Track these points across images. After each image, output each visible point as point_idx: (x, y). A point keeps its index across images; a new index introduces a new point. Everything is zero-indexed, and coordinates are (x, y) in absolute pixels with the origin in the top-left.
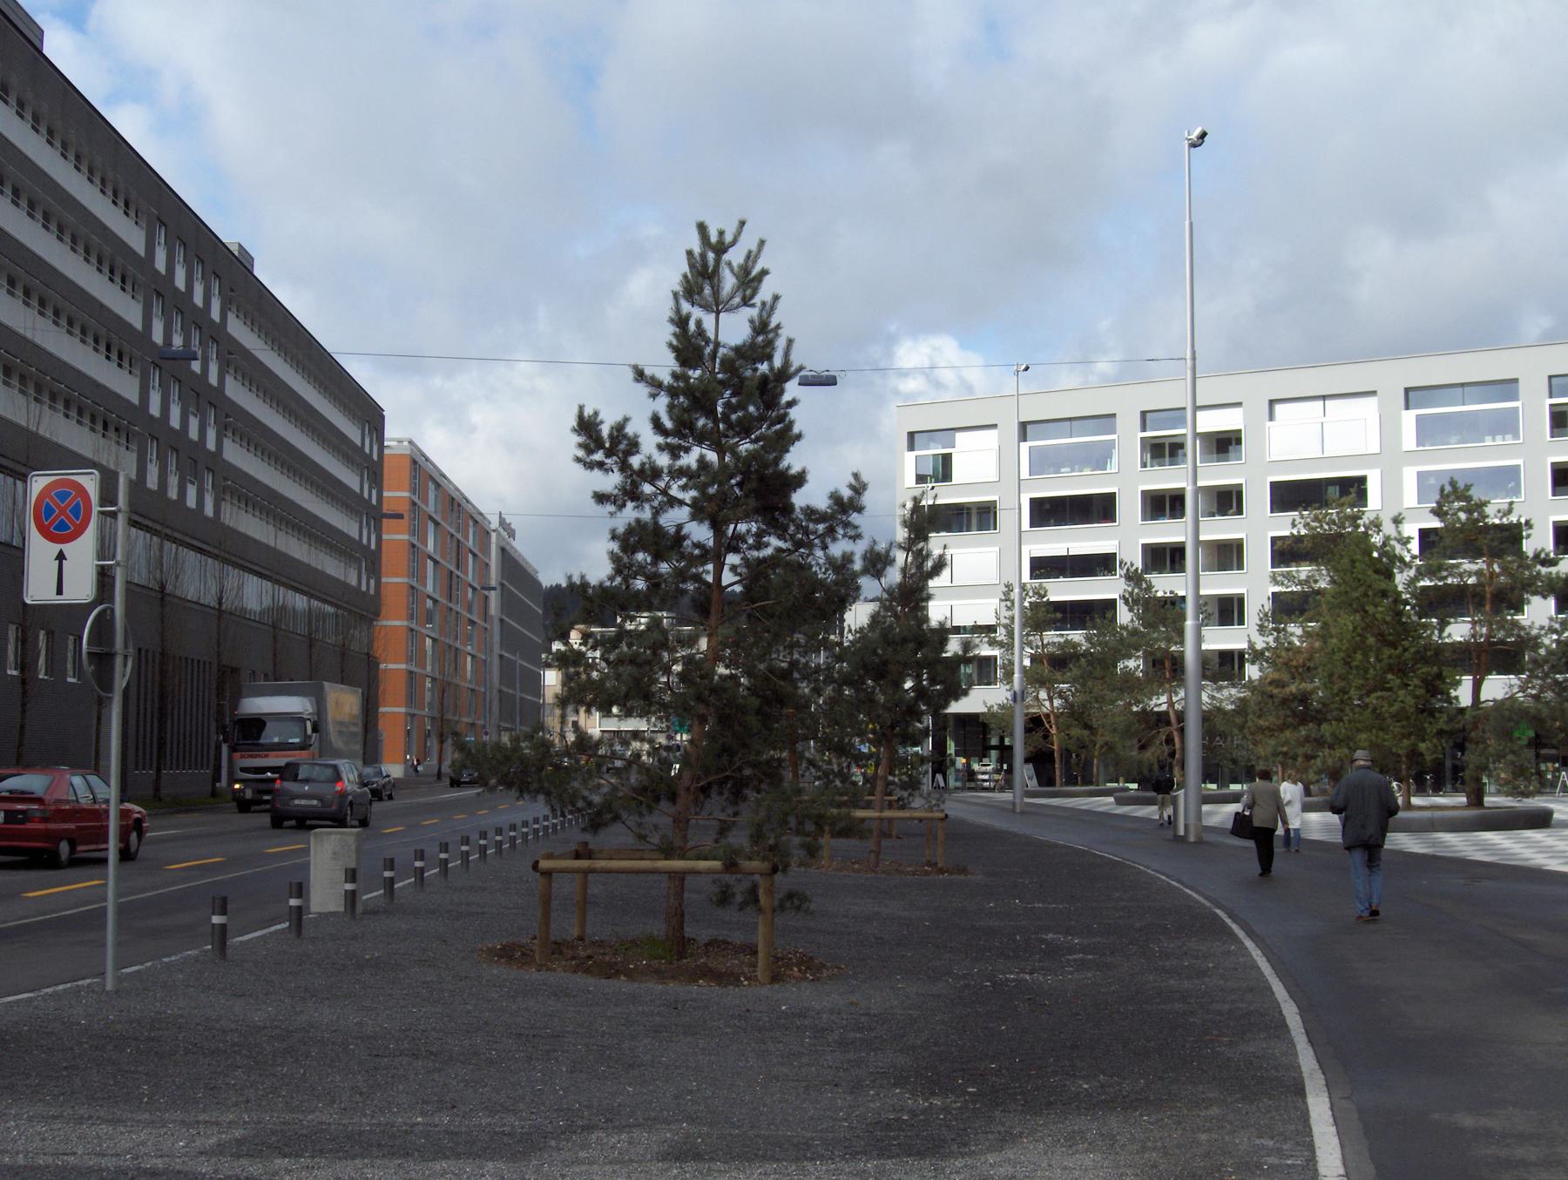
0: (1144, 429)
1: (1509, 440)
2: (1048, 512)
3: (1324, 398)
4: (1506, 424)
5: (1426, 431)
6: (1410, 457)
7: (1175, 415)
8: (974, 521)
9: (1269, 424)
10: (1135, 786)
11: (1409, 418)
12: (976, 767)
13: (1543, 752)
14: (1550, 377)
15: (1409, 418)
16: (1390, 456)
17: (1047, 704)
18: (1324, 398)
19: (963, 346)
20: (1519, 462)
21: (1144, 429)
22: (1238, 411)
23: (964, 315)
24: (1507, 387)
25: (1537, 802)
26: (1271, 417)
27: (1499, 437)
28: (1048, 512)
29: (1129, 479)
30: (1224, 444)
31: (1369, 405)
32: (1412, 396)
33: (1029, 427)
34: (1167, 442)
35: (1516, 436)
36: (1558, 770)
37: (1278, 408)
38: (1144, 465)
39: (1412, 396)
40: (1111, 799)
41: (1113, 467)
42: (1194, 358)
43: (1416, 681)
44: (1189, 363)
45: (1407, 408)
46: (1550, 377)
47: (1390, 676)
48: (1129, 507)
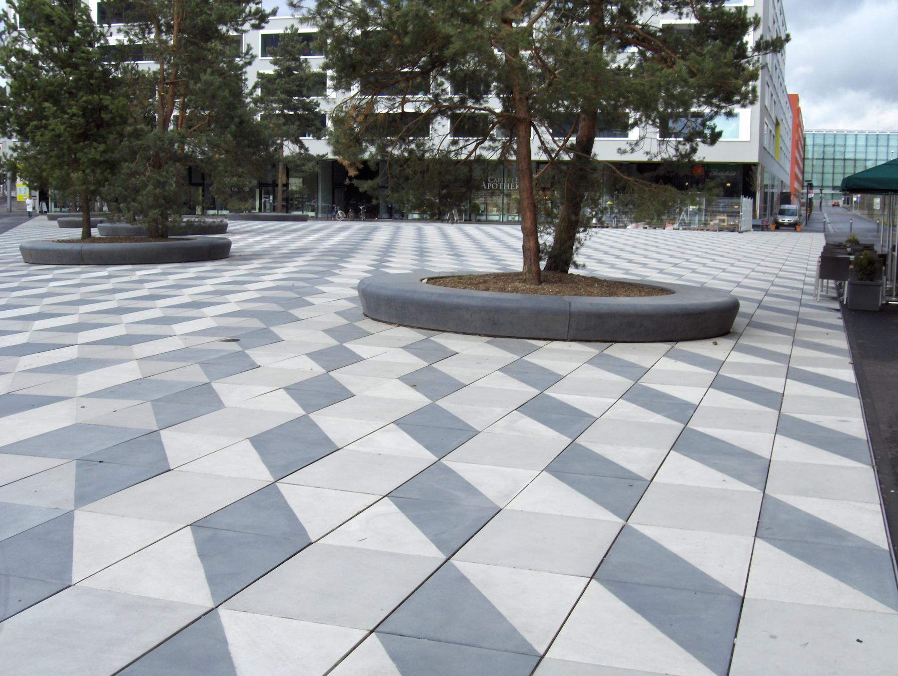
47: (46, 104)
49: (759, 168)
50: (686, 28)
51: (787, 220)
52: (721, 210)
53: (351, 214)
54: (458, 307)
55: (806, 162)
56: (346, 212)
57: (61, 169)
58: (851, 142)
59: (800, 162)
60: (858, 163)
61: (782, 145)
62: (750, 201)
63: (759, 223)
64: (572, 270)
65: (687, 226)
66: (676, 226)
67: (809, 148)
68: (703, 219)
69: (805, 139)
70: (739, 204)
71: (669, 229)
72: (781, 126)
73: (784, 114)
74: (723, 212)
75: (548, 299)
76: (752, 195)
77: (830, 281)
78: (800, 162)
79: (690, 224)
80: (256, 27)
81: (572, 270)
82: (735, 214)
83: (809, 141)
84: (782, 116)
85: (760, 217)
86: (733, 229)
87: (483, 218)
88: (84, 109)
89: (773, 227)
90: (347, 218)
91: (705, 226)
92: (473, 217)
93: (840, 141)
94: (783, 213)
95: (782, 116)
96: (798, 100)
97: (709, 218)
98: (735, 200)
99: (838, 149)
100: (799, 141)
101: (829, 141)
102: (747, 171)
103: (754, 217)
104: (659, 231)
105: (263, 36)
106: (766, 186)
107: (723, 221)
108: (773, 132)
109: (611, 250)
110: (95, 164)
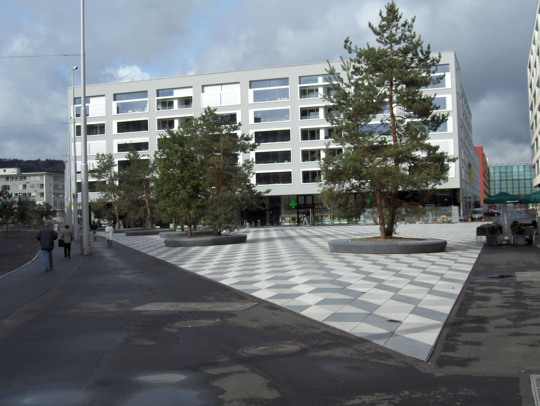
0: (158, 96)
1: (286, 100)
2: (123, 127)
3: (221, 84)
4: (284, 94)
5: (258, 96)
6: (252, 106)
7: (170, 91)
8: (98, 131)
9: (202, 94)
10: (159, 227)
11: (251, 92)
12: (102, 222)
13: (300, 211)
14: (300, 77)
15: (251, 92)
16: (244, 106)
17: (113, 198)
18: (221, 84)
19: (143, 71)
20: (289, 107)
21: (158, 96)
22: (191, 89)
23: (144, 60)
24: (285, 81)
25: (241, 231)
26: (203, 92)
27: (282, 99)
28: (123, 127)
29: (152, 114)
30: (187, 102)
31: (237, 88)
32: (252, 84)
33: (117, 96)
34: (167, 101)
35: (288, 99)
36: (304, 217)
37: (206, 88)
38: (158, 109)
39: (252, 84)
40: (124, 234)
41: (147, 110)
42: (84, 55)
43: (189, 186)
44: (82, 56)
45: (250, 88)
46: (300, 77)
47: (178, 185)
48: (153, 125)
49: (461, 191)
50: (457, 307)
51: (477, 216)
52: (443, 212)
53: (253, 224)
54: (365, 246)
55: (491, 183)
56: (251, 223)
57: (185, 209)
58: (515, 170)
59: (486, 183)
60: (521, 181)
61: (473, 176)
62: (457, 208)
63: (462, 218)
64: (394, 235)
65: (426, 222)
66: (421, 222)
67: (492, 175)
68: (434, 218)
69: (488, 170)
70: (451, 210)
71: (417, 224)
72: (472, 166)
73: (474, 160)
74: (444, 214)
75: (389, 241)
76: (458, 204)
77: (483, 237)
78: (486, 183)
79: (427, 221)
80: (252, 150)
81: (394, 235)
82: (450, 215)
83: (491, 171)
84: (473, 161)
85: (463, 215)
86: (449, 222)
87: (321, 223)
88: (192, 187)
89: (470, 220)
90: (251, 226)
91: (435, 221)
92: (316, 222)
93: (509, 170)
94: (475, 212)
95: (473, 161)
96: (482, 149)
97: (437, 217)
98: (449, 208)
99: (508, 174)
100: (486, 172)
101: (503, 170)
102: (455, 191)
103: (460, 215)
104: (413, 225)
105: (256, 153)
106: (465, 198)
107: (444, 218)
108: (468, 171)
109: (404, 230)
110: (198, 207)
